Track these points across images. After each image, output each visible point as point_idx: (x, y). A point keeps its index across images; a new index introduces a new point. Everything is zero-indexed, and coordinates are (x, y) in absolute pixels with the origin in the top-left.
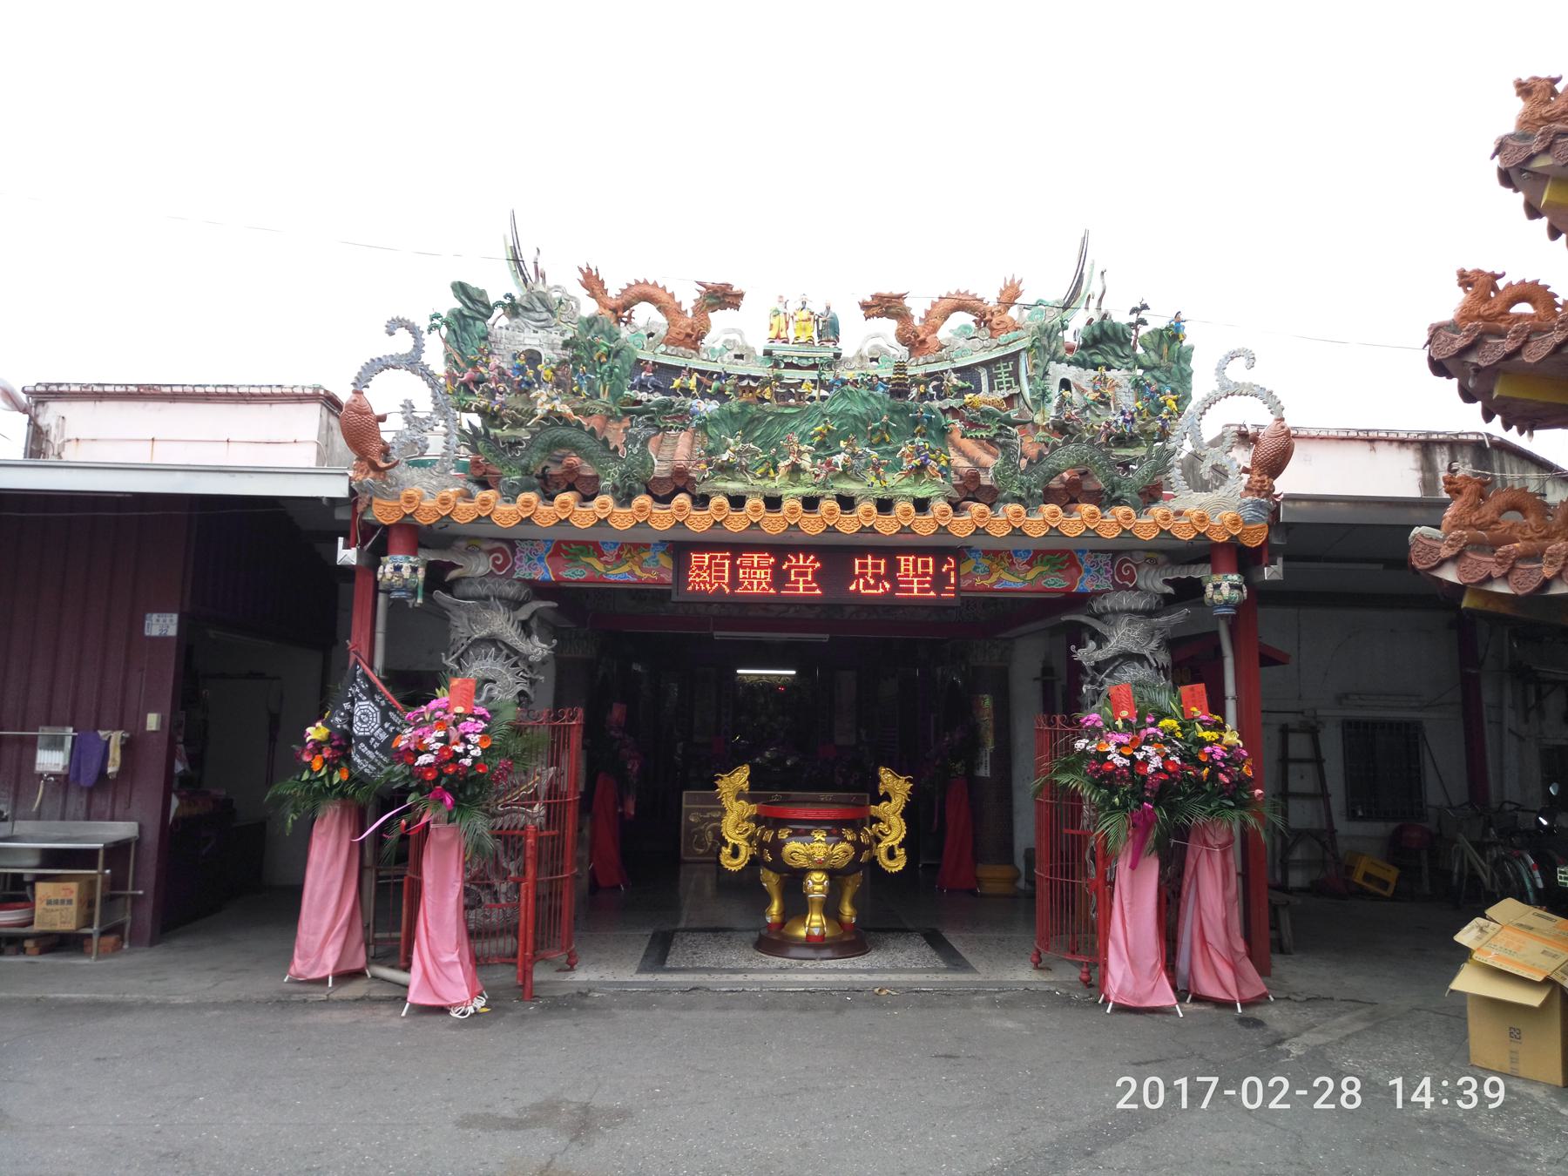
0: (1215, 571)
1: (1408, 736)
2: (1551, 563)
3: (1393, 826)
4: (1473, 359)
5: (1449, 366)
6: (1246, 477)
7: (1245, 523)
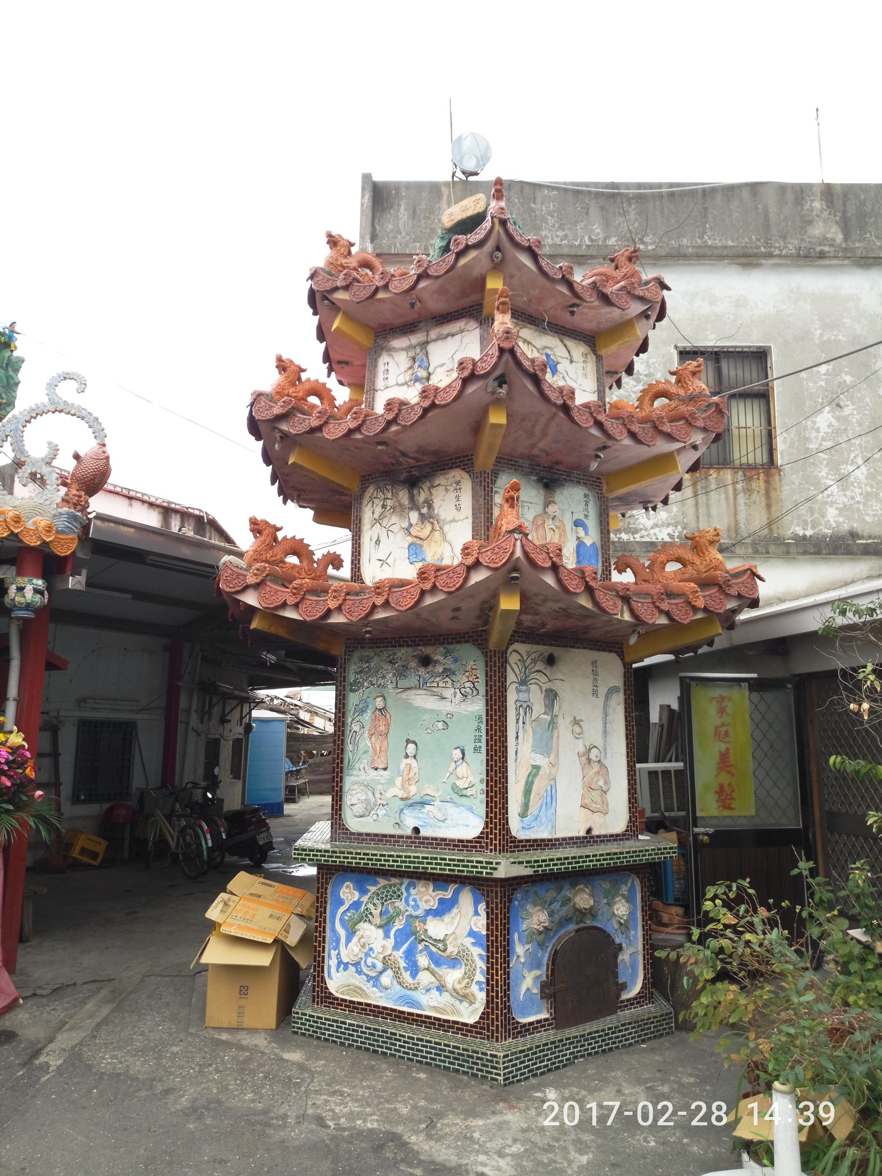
0: (19, 573)
1: (126, 731)
2: (335, 597)
3: (106, 806)
4: (284, 427)
5: (262, 428)
6: (63, 490)
7: (58, 532)
